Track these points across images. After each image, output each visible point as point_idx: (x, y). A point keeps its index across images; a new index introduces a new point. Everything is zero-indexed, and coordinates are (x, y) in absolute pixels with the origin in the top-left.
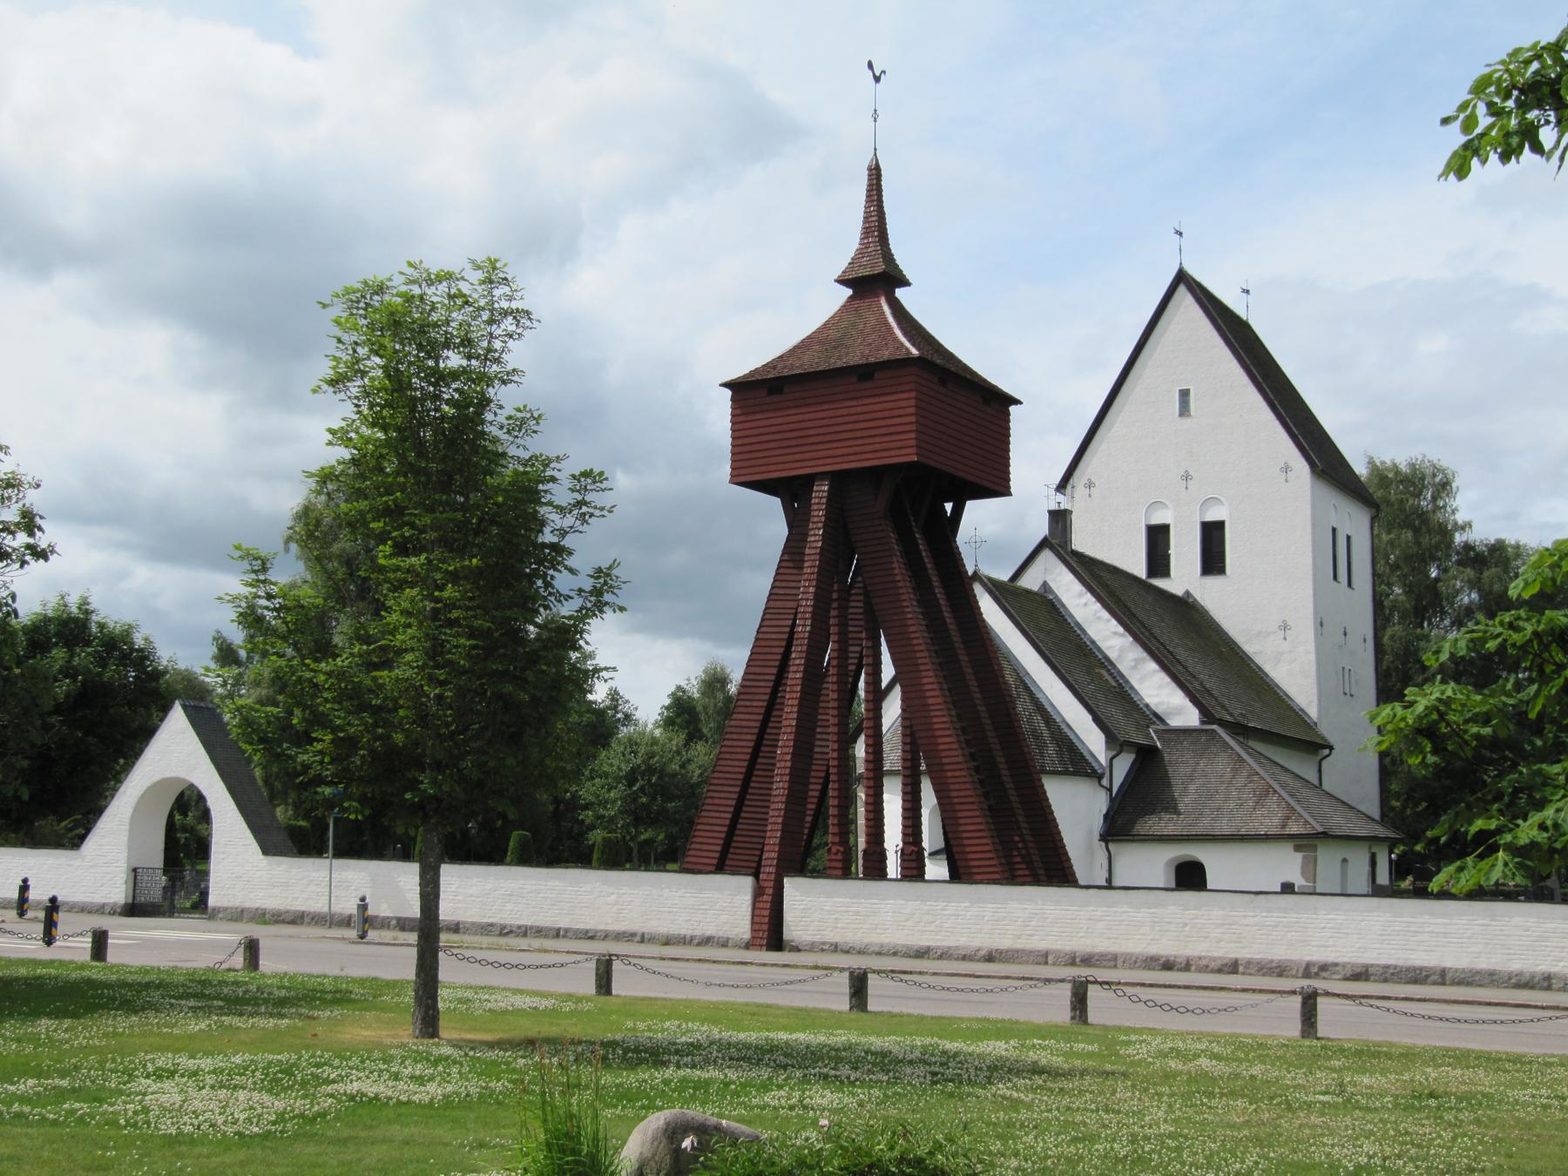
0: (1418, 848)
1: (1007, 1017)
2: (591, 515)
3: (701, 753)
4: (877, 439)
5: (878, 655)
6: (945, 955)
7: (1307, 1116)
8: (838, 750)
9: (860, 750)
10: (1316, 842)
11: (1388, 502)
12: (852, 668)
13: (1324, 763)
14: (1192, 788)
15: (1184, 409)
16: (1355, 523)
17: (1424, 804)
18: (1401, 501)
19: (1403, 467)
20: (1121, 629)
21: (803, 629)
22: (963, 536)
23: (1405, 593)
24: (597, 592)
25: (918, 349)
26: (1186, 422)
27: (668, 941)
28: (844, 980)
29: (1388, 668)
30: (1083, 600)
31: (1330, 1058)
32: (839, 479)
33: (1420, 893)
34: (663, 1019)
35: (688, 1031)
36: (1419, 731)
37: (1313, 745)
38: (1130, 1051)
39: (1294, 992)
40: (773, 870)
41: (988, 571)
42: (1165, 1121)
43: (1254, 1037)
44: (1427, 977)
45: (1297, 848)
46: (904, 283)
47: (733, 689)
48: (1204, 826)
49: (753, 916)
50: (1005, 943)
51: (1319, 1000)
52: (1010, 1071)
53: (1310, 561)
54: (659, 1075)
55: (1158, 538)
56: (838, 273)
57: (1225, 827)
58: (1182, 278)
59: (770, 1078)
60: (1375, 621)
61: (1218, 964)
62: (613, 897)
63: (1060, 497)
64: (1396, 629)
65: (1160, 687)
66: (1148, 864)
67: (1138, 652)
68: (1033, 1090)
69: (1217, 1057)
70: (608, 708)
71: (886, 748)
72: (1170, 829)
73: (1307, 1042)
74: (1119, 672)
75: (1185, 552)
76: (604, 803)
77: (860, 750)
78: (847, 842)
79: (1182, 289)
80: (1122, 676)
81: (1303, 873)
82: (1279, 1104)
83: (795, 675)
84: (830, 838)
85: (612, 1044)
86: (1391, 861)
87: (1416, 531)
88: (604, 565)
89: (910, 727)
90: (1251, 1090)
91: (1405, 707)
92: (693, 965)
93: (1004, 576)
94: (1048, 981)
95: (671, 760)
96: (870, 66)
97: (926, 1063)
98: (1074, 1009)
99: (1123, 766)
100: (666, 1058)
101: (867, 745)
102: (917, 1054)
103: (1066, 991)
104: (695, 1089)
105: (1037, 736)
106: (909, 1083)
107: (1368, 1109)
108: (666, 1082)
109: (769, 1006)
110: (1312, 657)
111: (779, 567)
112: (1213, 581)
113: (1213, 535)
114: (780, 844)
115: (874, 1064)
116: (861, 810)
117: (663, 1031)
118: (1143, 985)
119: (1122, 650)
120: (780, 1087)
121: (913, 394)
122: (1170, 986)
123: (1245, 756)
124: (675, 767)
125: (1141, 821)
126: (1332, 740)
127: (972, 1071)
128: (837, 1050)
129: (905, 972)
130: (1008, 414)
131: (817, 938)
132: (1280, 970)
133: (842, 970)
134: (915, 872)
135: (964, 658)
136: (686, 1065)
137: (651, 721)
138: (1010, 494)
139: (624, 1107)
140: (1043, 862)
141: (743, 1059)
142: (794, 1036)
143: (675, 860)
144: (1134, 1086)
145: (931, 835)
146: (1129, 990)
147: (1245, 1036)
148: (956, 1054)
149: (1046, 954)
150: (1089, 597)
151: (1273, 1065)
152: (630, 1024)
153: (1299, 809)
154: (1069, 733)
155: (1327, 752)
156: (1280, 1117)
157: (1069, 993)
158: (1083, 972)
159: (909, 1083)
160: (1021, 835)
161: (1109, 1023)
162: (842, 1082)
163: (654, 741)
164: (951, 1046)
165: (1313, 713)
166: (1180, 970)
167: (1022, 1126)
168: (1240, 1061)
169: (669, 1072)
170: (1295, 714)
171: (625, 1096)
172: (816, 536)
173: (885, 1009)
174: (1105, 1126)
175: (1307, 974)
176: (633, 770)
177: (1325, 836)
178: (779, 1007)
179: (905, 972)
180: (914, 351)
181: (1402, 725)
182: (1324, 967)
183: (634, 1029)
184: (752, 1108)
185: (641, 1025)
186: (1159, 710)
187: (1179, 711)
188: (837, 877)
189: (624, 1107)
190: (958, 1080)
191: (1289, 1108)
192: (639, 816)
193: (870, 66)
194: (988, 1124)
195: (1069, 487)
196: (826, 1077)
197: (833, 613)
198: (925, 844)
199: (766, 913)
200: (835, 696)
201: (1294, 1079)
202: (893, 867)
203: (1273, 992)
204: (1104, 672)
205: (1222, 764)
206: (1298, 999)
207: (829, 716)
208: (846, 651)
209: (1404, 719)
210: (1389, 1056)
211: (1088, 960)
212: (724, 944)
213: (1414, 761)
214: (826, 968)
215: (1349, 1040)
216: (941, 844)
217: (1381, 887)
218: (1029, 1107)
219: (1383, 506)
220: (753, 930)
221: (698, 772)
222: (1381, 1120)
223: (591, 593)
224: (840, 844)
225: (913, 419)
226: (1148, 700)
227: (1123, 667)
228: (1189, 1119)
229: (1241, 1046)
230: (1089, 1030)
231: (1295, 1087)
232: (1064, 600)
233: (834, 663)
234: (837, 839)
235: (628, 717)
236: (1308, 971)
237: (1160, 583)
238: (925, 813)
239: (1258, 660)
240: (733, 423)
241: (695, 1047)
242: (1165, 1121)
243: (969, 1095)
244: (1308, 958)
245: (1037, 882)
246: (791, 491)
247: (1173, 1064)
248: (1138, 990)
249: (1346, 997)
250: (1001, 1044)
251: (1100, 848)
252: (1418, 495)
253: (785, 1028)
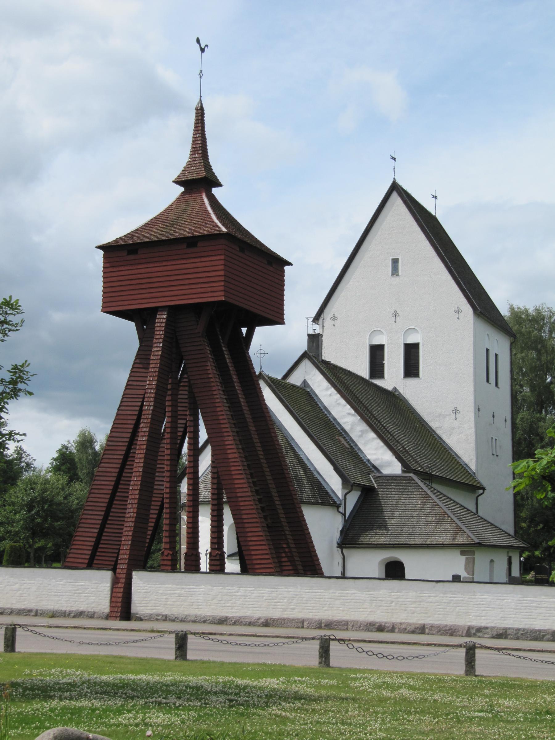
0: (537, 553)
1: (278, 662)
2: (10, 330)
3: (79, 489)
4: (199, 286)
5: (197, 426)
6: (237, 622)
7: (470, 726)
8: (170, 487)
9: (184, 487)
10: (474, 549)
11: (521, 333)
12: (180, 434)
13: (480, 498)
14: (397, 514)
15: (395, 271)
16: (501, 346)
17: (541, 526)
18: (529, 333)
19: (531, 311)
20: (352, 411)
21: (148, 408)
22: (254, 350)
23: (531, 391)
24: (13, 382)
25: (226, 228)
26: (396, 279)
27: (54, 615)
28: (172, 638)
29: (520, 439)
30: (329, 392)
31: (483, 689)
32: (174, 311)
33: (539, 582)
34: (51, 667)
35: (67, 675)
36: (544, 477)
37: (473, 488)
38: (357, 684)
39: (460, 646)
40: (125, 566)
41: (268, 372)
42: (380, 730)
43: (436, 675)
44: (544, 636)
45: (462, 553)
46: (219, 185)
47: (97, 447)
48: (404, 538)
49: (112, 597)
50: (276, 614)
51: (477, 651)
52: (280, 698)
53: (472, 369)
54: (47, 705)
55: (377, 353)
56: (175, 176)
57: (417, 539)
58: (395, 187)
59: (122, 706)
60: (512, 408)
61: (413, 627)
62: (17, 586)
63: (315, 326)
64: (524, 414)
65: (376, 449)
66: (368, 562)
67: (363, 426)
68: (295, 710)
69: (411, 687)
70: (16, 459)
71: (201, 486)
72: (382, 540)
73: (469, 678)
74: (351, 438)
75: (394, 362)
76: (11, 523)
77: (184, 487)
78: (175, 548)
79: (395, 195)
80: (353, 441)
81: (466, 569)
82: (452, 718)
83: (143, 438)
84: (163, 545)
85: (14, 685)
86: (520, 561)
87: (539, 352)
88: (20, 363)
89: (217, 473)
90: (434, 710)
91: (535, 462)
92: (70, 630)
93: (279, 377)
94: (304, 639)
95: (58, 494)
96: (198, 41)
97: (225, 693)
98: (321, 657)
99: (353, 499)
100: (52, 693)
101: (189, 484)
102: (220, 687)
103: (316, 646)
104: (72, 714)
105: (299, 480)
106: (215, 707)
107: (508, 722)
108: (52, 710)
109: (121, 657)
110: (473, 431)
111: (133, 368)
112: (411, 381)
113: (411, 352)
114: (131, 549)
115: (192, 695)
116: (184, 527)
117: (50, 675)
118: (364, 641)
119: (353, 425)
120: (129, 711)
121: (222, 257)
122: (382, 642)
123: (430, 493)
124: (60, 498)
125: (364, 535)
126: (484, 482)
127: (255, 698)
128: (167, 686)
129: (211, 634)
130: (284, 271)
131: (154, 612)
132: (451, 631)
133: (170, 632)
134: (218, 568)
135: (252, 428)
136: (66, 698)
137: (45, 467)
138: (284, 323)
139: (23, 728)
140: (300, 561)
141: (104, 693)
142: (139, 677)
143: (59, 561)
144: (360, 707)
145: (229, 544)
146: (356, 645)
147: (430, 674)
148: (245, 688)
149: (303, 621)
150: (332, 390)
151: (448, 693)
152: (27, 671)
153: (463, 527)
154: (319, 478)
155: (481, 491)
156: (453, 727)
157: (318, 647)
158: (327, 633)
159: (215, 707)
160: (288, 544)
161: (344, 666)
162: (170, 707)
163: (47, 482)
164: (241, 682)
165: (473, 466)
166: (388, 631)
167: (288, 734)
168: (427, 690)
169: (54, 703)
170: (462, 468)
171: (24, 720)
172: (158, 348)
173: (199, 658)
174: (342, 734)
175: (468, 634)
176: (32, 501)
177: (480, 545)
178: (129, 658)
179: (211, 634)
180: (224, 229)
181: (533, 473)
182: (479, 630)
183: (30, 675)
184: (111, 726)
185: (35, 672)
186: (376, 464)
187: (389, 464)
188: (167, 571)
189: (23, 728)
190: (246, 704)
191: (459, 721)
192: (36, 531)
193: (198, 41)
194: (267, 733)
195: (321, 319)
196: (160, 703)
197: (168, 398)
198: (225, 549)
199: (120, 595)
200: (168, 452)
201: (461, 702)
202: (204, 565)
203: (447, 646)
204: (341, 439)
205: (416, 499)
206: (464, 650)
207: (165, 466)
208: (176, 422)
209: (534, 469)
210: (520, 687)
211: (329, 625)
212: (91, 616)
213: (541, 496)
214: (159, 632)
215: (495, 677)
216: (236, 549)
217: (515, 578)
218: (293, 721)
219: (518, 336)
220: (111, 607)
221: (76, 502)
222: (516, 729)
223: (10, 383)
224: (170, 549)
225: (222, 273)
226: (369, 457)
227: (354, 435)
228: (395, 728)
229: (427, 681)
230: (331, 671)
231: (462, 707)
232: (317, 392)
233: (168, 430)
234: (168, 546)
235: (28, 465)
236: (470, 632)
237: (378, 382)
238: (226, 529)
239: (439, 432)
240: (104, 272)
241: (72, 686)
242: (380, 730)
243: (254, 714)
244: (469, 624)
245: (297, 573)
246: (142, 318)
247: (385, 693)
248: (361, 644)
249: (498, 649)
250: (274, 680)
251: (337, 552)
252: (540, 329)
253: (132, 672)
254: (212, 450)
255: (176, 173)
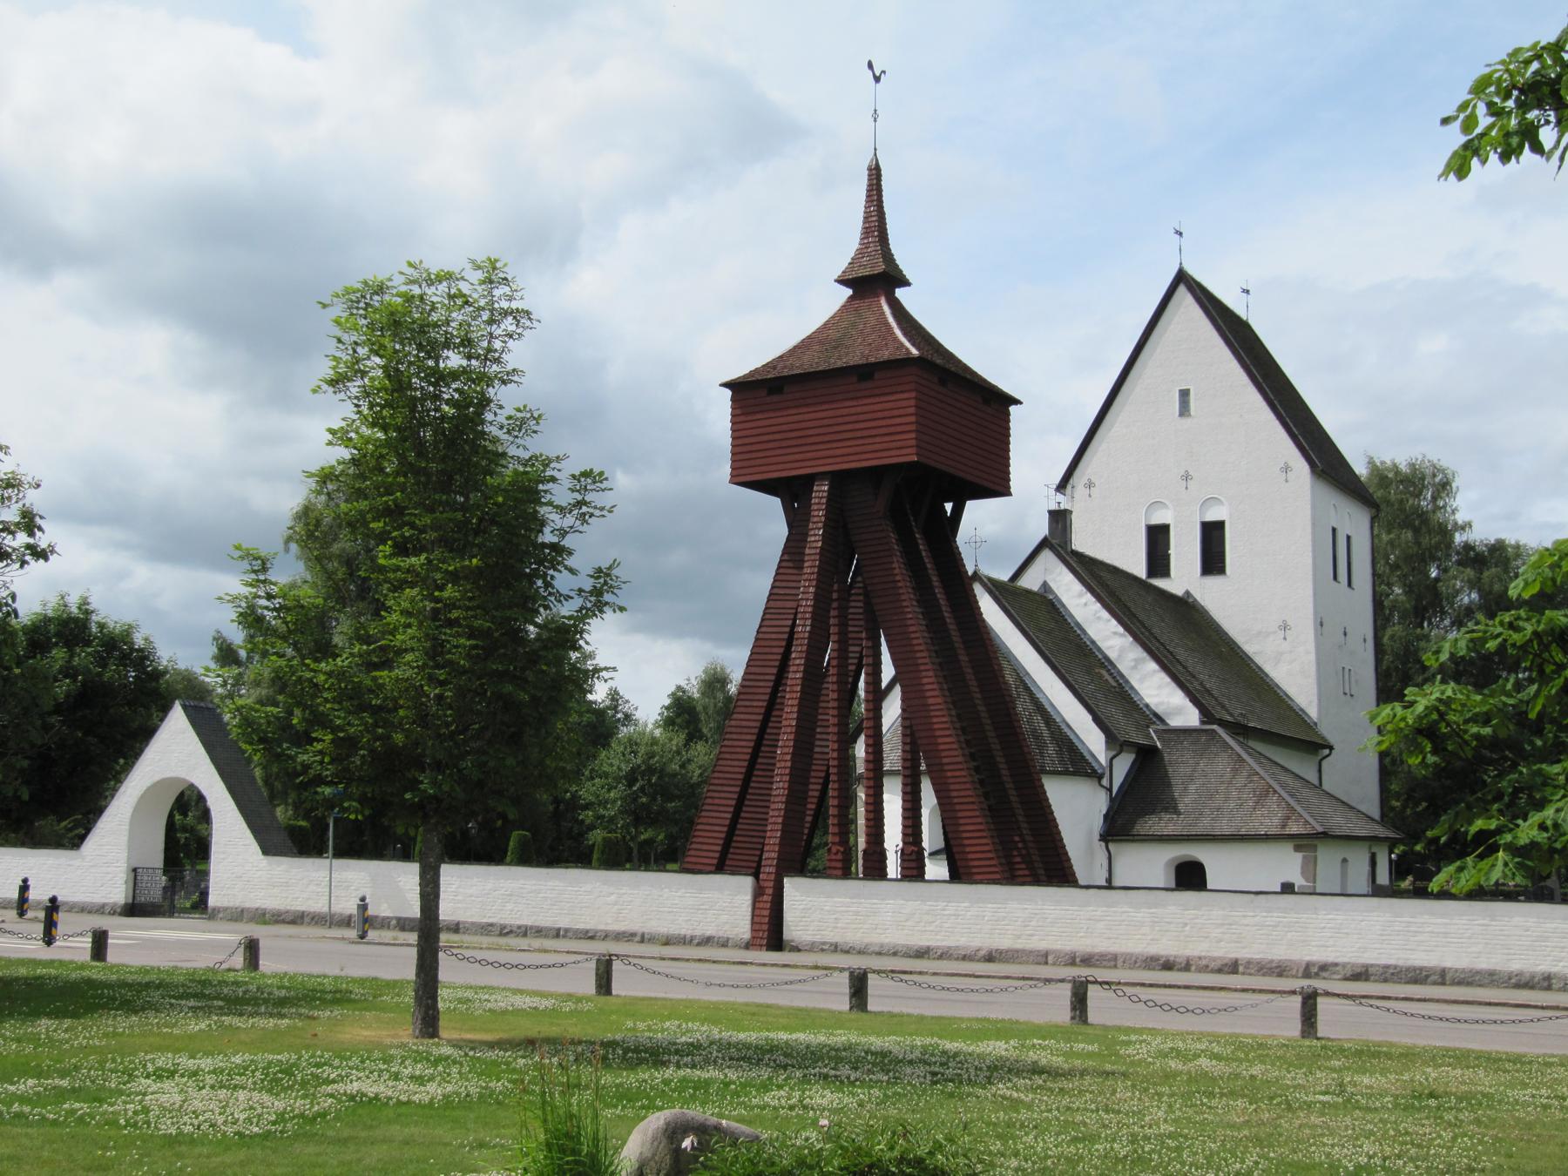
0: (1418, 848)
1: (1007, 1017)
2: (591, 515)
3: (701, 753)
4: (877, 439)
5: (878, 655)
6: (945, 955)
7: (1307, 1116)
8: (838, 750)
9: (860, 750)
10: (1316, 842)
11: (1388, 502)
12: (852, 668)
13: (1324, 763)
14: (1192, 788)
15: (1184, 409)
16: (1355, 523)
17: (1424, 804)
18: (1401, 501)
19: (1403, 467)
20: (1121, 629)
21: (803, 629)
22: (963, 536)
23: (1405, 593)
24: (597, 592)
25: (918, 349)
26: (1186, 422)
27: (668, 941)
28: (844, 980)
29: (1388, 668)
30: (1083, 600)
31: (1330, 1058)
32: (839, 479)
33: (1420, 893)
34: (663, 1019)
35: (688, 1031)
36: (1419, 731)
37: (1313, 745)
38: (1130, 1051)
39: (1294, 992)
40: (773, 870)
41: (988, 571)
42: (1165, 1121)
43: (1254, 1037)
44: (1427, 977)
45: (1297, 848)
46: (904, 283)
47: (733, 689)
48: (1204, 826)
49: (753, 916)
50: (1005, 943)
51: (1319, 1000)
52: (1010, 1071)
53: (1310, 561)
54: (659, 1075)
55: (1158, 538)
56: (838, 273)
57: (1225, 827)
58: (1182, 278)
59: (770, 1078)
60: (1375, 621)
61: (1218, 964)
62: (613, 897)
63: (1060, 497)
64: (1396, 629)
65: (1160, 687)
66: (1148, 864)
67: (1138, 652)
68: (1033, 1090)
69: (1217, 1057)
70: (608, 708)
71: (886, 748)
72: (1170, 829)
73: (1307, 1042)
74: (1119, 672)
75: (1185, 552)
76: (604, 803)
77: (860, 750)
78: (847, 842)
79: (1182, 289)
80: (1122, 676)
81: (1303, 873)
82: (1279, 1104)
83: (795, 675)
84: (830, 838)
85: (612, 1044)
86: (1391, 861)
87: (1416, 531)
88: (604, 565)
89: (910, 727)
90: (1251, 1090)
91: (1405, 707)
92: (693, 965)
93: (1004, 576)
94: (1048, 981)
95: (671, 760)
96: (870, 66)
97: (926, 1063)
98: (1074, 1009)
99: (1123, 766)
100: (666, 1058)
101: (867, 745)
102: (917, 1054)
103: (1066, 991)
104: (695, 1089)
105: (1037, 736)
106: (909, 1083)
107: (1368, 1109)
108: (666, 1082)
109: (769, 1006)
110: (1312, 657)
111: (779, 567)
112: (1213, 581)
113: (1213, 535)
114: (780, 844)
115: (874, 1064)
116: (861, 810)
117: (663, 1031)
118: (1143, 985)
119: (1122, 650)
120: (780, 1087)
121: (913, 394)
122: (1170, 986)
123: (1245, 756)
124: (675, 767)
125: (1141, 821)
126: (1332, 740)
127: (972, 1071)
128: (837, 1050)
129: (905, 972)
130: (1008, 414)
131: (817, 938)
132: (1280, 970)
133: (842, 970)
134: (915, 872)
135: (964, 658)
136: (686, 1065)
137: (651, 721)
138: (1010, 494)
139: (624, 1107)
140: (1043, 862)
141: (743, 1059)
142: (794, 1036)
143: (675, 860)
144: (1134, 1086)
145: (931, 835)
146: (1129, 990)
147: (1245, 1036)
148: (956, 1054)
149: (1046, 954)
150: (1089, 597)
151: (1273, 1065)
152: (630, 1024)
153: (1299, 809)
154: (1069, 733)
155: (1327, 752)
156: (1280, 1117)
157: (1069, 993)
158: (1083, 972)
159: (909, 1083)
160: (1021, 835)
161: (1109, 1023)
162: (842, 1082)
163: (654, 741)
164: (951, 1046)
165: (1313, 713)
166: (1180, 970)
167: (1022, 1126)
168: (1240, 1061)
169: (669, 1072)
170: (1295, 714)
171: (625, 1096)
172: (816, 536)
173: (885, 1009)
174: (1105, 1126)
175: (1307, 974)
176: (633, 770)
177: (1325, 836)
178: (779, 1007)
179: (905, 972)
180: (914, 351)
181: (1402, 725)
182: (1324, 967)
183: (634, 1029)
184: (752, 1108)
185: (641, 1025)
186: (1159, 710)
187: (1179, 711)
188: (837, 877)
189: (624, 1107)
190: (958, 1080)
191: (1289, 1108)
192: (639, 816)
193: (870, 66)
194: (988, 1124)
195: (1069, 487)
196: (826, 1077)
197: (833, 613)
198: (925, 844)
199: (766, 913)
200: (835, 696)
201: (1294, 1079)
202: (893, 867)
203: (1273, 992)
204: (1104, 672)
205: (1222, 764)
206: (1298, 999)
207: (829, 716)
208: (846, 651)
209: (1404, 719)
210: (1389, 1056)
211: (1088, 960)
212: (724, 944)
213: (1414, 761)
214: (826, 968)
215: (1349, 1040)
216: (941, 844)
217: (1381, 887)
218: (1029, 1107)
219: (1383, 506)
220: (753, 930)
221: (698, 772)
222: (1381, 1120)
223: (591, 593)
224: (840, 844)
225: (913, 419)
226: (1148, 700)
227: (1123, 667)
228: (1189, 1119)
229: (1241, 1046)
230: (1089, 1030)
231: (1295, 1087)
232: (1064, 600)
233: (834, 663)
234: (837, 839)
235: (628, 717)
236: (1308, 971)
237: (1160, 583)
238: (925, 813)
239: (1258, 660)
240: (733, 423)
241: (695, 1047)
242: (1165, 1121)
243: (969, 1095)
244: (1308, 958)
245: (1037, 882)
246: (791, 491)
247: (1173, 1064)
248: (1138, 990)
249: (1346, 997)
250: (1001, 1044)
251: (1100, 848)
252: (1418, 495)
253: (785, 1028)
254: (903, 700)
255: (841, 264)
